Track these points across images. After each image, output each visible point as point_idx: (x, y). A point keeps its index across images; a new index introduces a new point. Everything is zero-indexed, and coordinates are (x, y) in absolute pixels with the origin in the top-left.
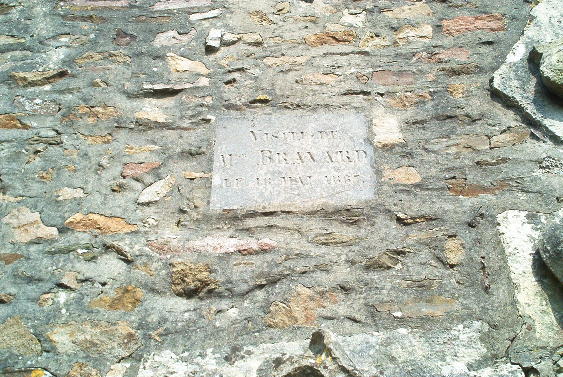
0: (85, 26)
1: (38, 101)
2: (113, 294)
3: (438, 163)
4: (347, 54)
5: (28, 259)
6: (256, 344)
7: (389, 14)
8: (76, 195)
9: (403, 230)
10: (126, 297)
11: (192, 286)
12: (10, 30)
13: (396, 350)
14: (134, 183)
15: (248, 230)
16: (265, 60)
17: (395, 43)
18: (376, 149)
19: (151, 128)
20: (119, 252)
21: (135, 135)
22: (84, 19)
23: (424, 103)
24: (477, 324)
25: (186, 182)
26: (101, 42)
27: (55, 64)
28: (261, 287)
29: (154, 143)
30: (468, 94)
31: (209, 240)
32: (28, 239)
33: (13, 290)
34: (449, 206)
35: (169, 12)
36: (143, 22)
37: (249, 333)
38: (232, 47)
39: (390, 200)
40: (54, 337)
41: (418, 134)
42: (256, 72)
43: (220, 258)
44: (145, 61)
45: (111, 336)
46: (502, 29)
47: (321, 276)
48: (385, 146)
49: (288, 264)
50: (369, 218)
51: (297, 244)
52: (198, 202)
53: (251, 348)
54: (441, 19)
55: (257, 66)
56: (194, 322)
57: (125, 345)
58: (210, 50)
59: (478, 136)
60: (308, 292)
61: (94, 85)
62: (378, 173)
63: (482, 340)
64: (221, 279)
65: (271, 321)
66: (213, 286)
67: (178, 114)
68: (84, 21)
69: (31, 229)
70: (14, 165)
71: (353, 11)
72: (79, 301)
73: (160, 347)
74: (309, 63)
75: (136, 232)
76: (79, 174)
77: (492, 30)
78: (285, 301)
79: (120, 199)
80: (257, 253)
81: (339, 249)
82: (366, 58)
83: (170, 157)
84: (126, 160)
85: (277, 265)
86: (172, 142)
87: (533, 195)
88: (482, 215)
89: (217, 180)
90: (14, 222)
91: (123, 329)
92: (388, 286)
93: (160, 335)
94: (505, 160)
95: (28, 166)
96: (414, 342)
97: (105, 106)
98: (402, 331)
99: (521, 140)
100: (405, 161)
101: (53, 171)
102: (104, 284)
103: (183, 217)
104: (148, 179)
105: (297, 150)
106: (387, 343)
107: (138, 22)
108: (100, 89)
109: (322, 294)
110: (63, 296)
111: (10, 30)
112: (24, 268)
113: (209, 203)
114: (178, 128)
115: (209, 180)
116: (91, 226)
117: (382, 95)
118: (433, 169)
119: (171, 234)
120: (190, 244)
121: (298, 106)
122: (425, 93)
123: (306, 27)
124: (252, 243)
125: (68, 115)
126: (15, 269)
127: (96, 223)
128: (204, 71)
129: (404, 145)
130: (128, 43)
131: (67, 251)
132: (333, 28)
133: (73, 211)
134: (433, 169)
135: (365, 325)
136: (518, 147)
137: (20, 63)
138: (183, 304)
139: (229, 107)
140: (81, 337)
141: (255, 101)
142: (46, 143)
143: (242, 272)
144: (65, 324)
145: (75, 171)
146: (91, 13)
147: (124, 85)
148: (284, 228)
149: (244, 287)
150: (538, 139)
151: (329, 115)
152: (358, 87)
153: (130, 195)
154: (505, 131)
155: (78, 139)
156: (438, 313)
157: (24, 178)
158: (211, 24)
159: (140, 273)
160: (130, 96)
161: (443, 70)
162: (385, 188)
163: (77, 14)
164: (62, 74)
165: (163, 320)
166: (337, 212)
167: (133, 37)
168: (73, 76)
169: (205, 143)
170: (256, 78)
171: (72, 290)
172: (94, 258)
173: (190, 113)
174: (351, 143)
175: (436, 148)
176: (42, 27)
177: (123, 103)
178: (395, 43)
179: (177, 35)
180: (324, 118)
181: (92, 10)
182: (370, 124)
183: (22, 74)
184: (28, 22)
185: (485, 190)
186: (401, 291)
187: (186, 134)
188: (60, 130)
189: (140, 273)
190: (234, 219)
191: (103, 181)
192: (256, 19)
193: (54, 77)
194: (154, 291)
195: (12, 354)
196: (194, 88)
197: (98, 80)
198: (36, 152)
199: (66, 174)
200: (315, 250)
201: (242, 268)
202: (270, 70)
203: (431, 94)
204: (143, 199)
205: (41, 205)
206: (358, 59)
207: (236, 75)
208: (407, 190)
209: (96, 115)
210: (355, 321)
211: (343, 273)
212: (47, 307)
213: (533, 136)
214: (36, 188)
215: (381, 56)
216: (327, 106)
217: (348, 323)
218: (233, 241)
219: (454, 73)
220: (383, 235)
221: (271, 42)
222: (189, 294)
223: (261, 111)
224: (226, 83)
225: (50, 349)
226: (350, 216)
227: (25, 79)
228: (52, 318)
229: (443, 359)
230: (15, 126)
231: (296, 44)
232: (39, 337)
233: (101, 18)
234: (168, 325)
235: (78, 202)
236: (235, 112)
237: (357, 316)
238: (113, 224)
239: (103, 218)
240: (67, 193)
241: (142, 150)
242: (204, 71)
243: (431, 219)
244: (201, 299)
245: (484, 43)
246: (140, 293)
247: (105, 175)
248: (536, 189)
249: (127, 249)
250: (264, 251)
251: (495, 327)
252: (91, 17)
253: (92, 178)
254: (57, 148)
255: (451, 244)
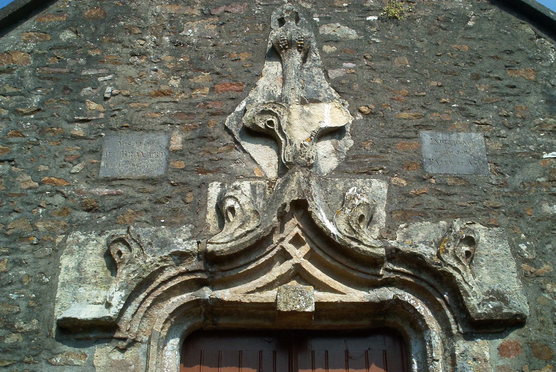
0: (49, 83)
1: (29, 124)
2: (59, 210)
3: (194, 159)
4: (167, 102)
5: (27, 195)
6: (110, 230)
7: (192, 80)
8: (46, 169)
9: (172, 188)
10: (65, 211)
11: (90, 207)
12: (14, 84)
13: (160, 234)
14: (69, 164)
15: (113, 186)
16: (130, 104)
17: (191, 97)
18: (169, 152)
19: (77, 139)
20: (62, 193)
21: (70, 142)
22: (49, 79)
23: (196, 129)
24: (190, 225)
25: (90, 164)
26: (56, 93)
27: (35, 104)
28: (115, 209)
29: (78, 146)
30: (215, 126)
31: (98, 190)
32: (27, 187)
33: (22, 208)
34: (194, 179)
35: (89, 76)
36: (76, 81)
37: (109, 226)
38: (116, 97)
39: (170, 175)
40: (38, 226)
41: (190, 145)
42: (126, 111)
43: (101, 197)
44: (76, 104)
45: (58, 226)
46: (241, 91)
47: (138, 205)
48: (174, 150)
49: (127, 200)
50: (161, 182)
51: (131, 192)
52: (94, 173)
53: (108, 231)
54: (215, 84)
55: (126, 107)
56: (89, 221)
57: (63, 229)
58: (106, 99)
59: (214, 147)
60: (132, 211)
61: (54, 116)
62: (168, 163)
63: (191, 231)
64: (100, 205)
65: (117, 222)
66: (97, 208)
67: (89, 132)
68: (49, 80)
69: (28, 183)
70: (20, 155)
71: (175, 77)
72: (47, 212)
73: (76, 230)
74: (150, 107)
75: (69, 185)
76: (47, 159)
77: (237, 91)
78: (123, 215)
79: (64, 171)
80: (115, 195)
81: (147, 195)
82: (176, 105)
83: (85, 153)
84: (66, 153)
85: (122, 200)
86: (86, 146)
87: (227, 175)
88: (204, 183)
89: (103, 164)
90: (21, 180)
91: (63, 223)
92: (162, 210)
93: (76, 226)
94: (221, 159)
95: (25, 155)
96: (166, 231)
97: (58, 128)
98: (163, 227)
99: (231, 150)
100: (181, 158)
101: (36, 158)
102: (56, 206)
103: (88, 179)
104: (75, 162)
105: (137, 151)
106: (156, 231)
107: (73, 81)
108: (55, 118)
109: (137, 212)
110: (41, 211)
111: (14, 84)
112: (25, 199)
113: (99, 174)
114: (89, 139)
115: (100, 164)
116: (51, 182)
117: (179, 125)
118: (191, 162)
119: (83, 187)
120: (90, 191)
121: (141, 130)
122: (196, 124)
123: (151, 87)
124: (114, 191)
125: (42, 131)
126: (22, 199)
127: (53, 181)
128: (102, 109)
129: (181, 150)
130: (69, 94)
131: (42, 192)
132: (163, 88)
133: (45, 176)
134: (191, 162)
135: (151, 224)
136: (228, 153)
137: (19, 103)
138: (86, 214)
139: (112, 129)
140: (48, 226)
141: (123, 127)
142: (32, 144)
143: (109, 203)
144: (42, 221)
145: (45, 158)
146: (52, 75)
147: (66, 117)
148: (127, 186)
149: (109, 209)
150: (237, 150)
151: (153, 135)
152: (169, 120)
153: (67, 169)
154: (225, 145)
155: (46, 142)
156: (178, 221)
157: (24, 160)
158: (108, 83)
159: (70, 202)
160: (69, 122)
161: (208, 112)
162: (169, 170)
163: (45, 76)
164: (39, 110)
165: (78, 220)
166: (148, 179)
167: (71, 90)
168: (44, 111)
169: (99, 147)
170: (125, 114)
171: (44, 208)
172: (53, 195)
173: (94, 132)
174: (160, 149)
175: (195, 152)
176: (29, 83)
177: (65, 125)
178: (191, 97)
179: (91, 90)
180: (152, 136)
181: (53, 73)
182: (169, 140)
183: (21, 109)
184: (22, 79)
185: (210, 172)
186: (166, 212)
187: (92, 142)
188: (39, 138)
189: (70, 202)
190: (108, 181)
191: (57, 163)
192: (130, 81)
193: (35, 111)
194: (75, 209)
195: (22, 231)
196: (98, 119)
197: (55, 114)
198: (29, 149)
199: (41, 159)
200: (137, 195)
201: (109, 201)
202: (132, 110)
203: (200, 125)
204: (73, 171)
205: (31, 173)
206: (172, 105)
207: (116, 112)
208: (178, 171)
209: (53, 131)
210: (147, 222)
211: (146, 204)
212: (35, 214)
213: (236, 149)
214: (29, 165)
215: (184, 104)
216: (153, 130)
217: (145, 223)
218: (107, 190)
219: (213, 114)
220: (166, 189)
221: (134, 95)
222: (88, 211)
223: (125, 132)
224: (111, 116)
225: (37, 230)
226: (152, 181)
227: (22, 112)
228: (37, 218)
229: (175, 237)
230: (19, 136)
231: (145, 96)
232: (32, 225)
233: (57, 79)
234: (79, 222)
235: (46, 172)
236: (114, 132)
237: (148, 221)
238: (60, 182)
239: (56, 179)
240: (42, 168)
241: (73, 149)
242: (102, 109)
243: (185, 184)
244: (93, 213)
245: (231, 99)
246: (70, 210)
247: (57, 160)
248: (229, 172)
249: (65, 192)
250: (119, 195)
251: (196, 227)
252: (52, 78)
253: (52, 161)
254: (37, 146)
255: (189, 195)
